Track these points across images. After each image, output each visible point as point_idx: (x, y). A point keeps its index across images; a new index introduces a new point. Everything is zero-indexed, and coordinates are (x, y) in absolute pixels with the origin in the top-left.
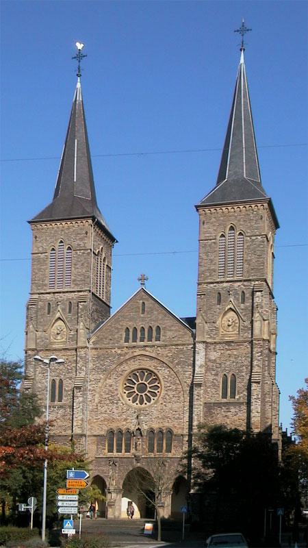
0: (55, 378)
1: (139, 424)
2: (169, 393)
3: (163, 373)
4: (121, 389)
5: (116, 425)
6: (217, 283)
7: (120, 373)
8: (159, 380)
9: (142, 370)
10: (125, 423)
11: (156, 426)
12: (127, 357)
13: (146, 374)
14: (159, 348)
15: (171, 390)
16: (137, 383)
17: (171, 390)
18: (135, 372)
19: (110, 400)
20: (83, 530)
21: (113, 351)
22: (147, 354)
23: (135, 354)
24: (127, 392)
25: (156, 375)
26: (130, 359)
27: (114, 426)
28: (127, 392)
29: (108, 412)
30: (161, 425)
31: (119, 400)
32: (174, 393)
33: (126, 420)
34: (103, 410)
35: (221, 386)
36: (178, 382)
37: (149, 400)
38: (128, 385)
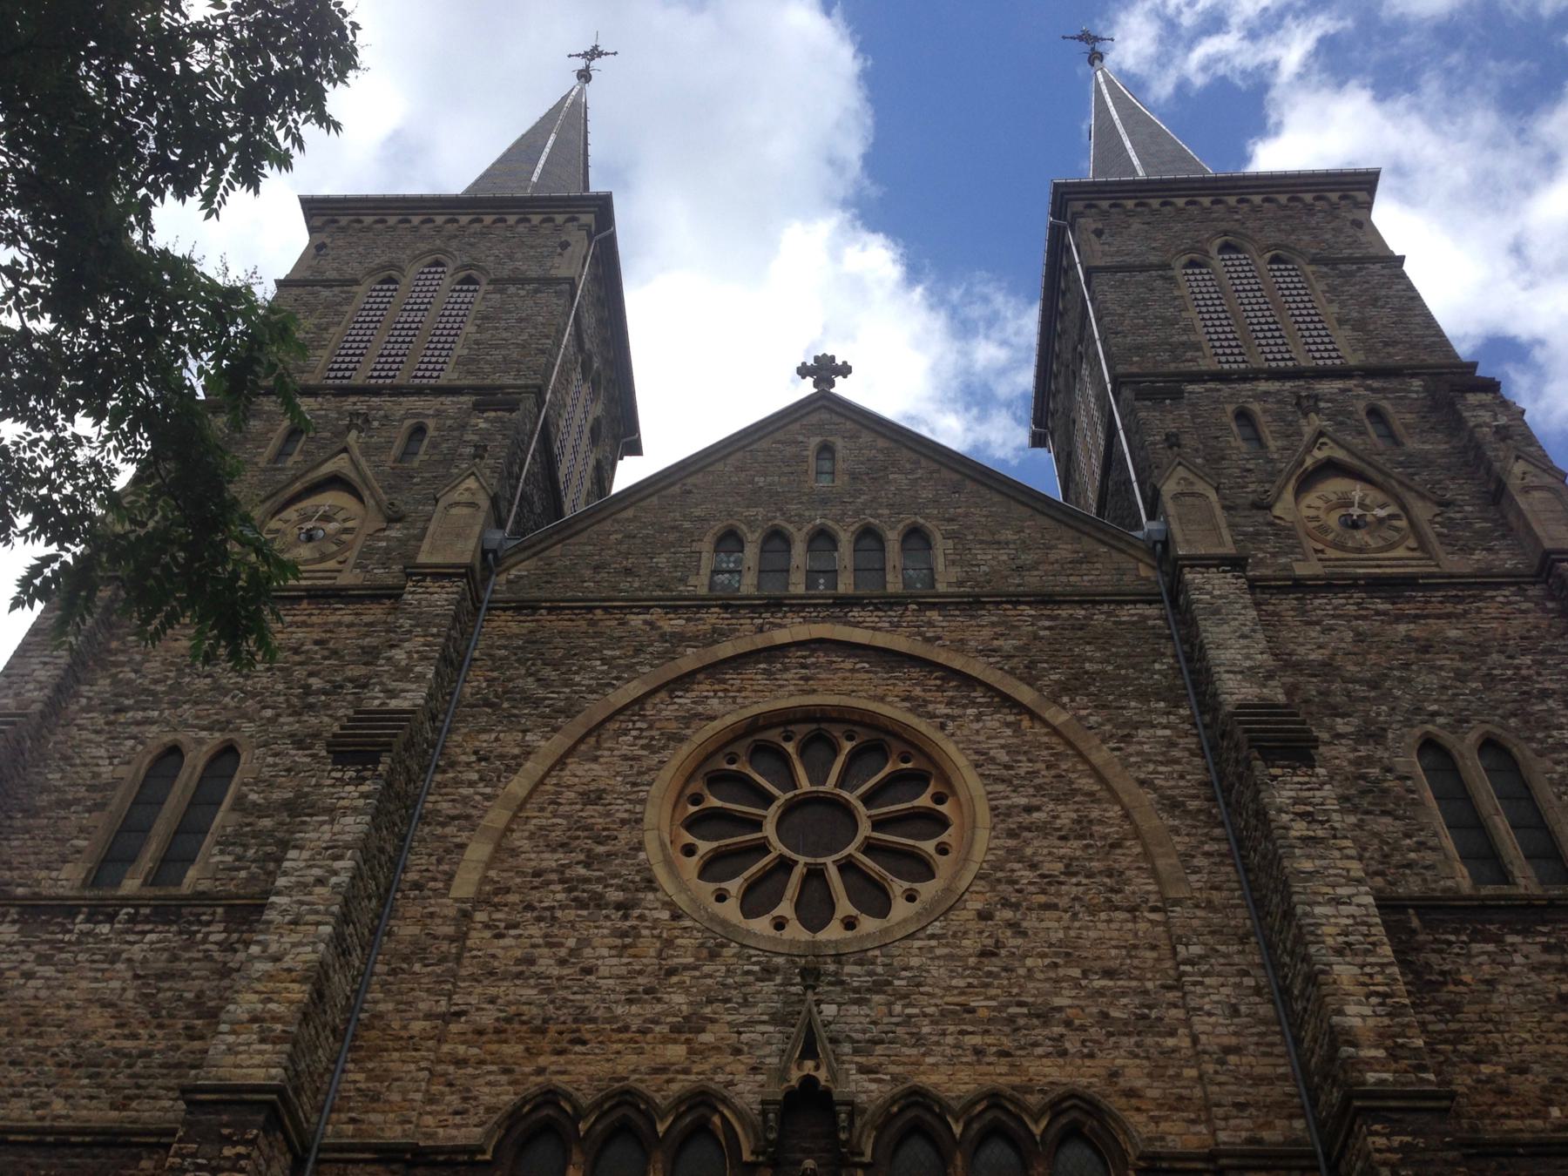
0: (184, 737)
1: (809, 1051)
2: (1036, 846)
3: (962, 742)
4: (659, 819)
5: (601, 1068)
6: (1089, 599)
7: (672, 727)
8: (946, 780)
9: (819, 730)
10: (676, 1052)
11: (953, 1080)
12: (726, 650)
13: (847, 746)
14: (934, 615)
15: (1043, 829)
16: (783, 797)
17: (1043, 829)
18: (774, 735)
19: (570, 885)
20: (1120, 369)
21: (636, 621)
22: (860, 636)
23: (781, 636)
24: (704, 847)
25: (913, 745)
26: (739, 661)
27: (583, 1074)
28: (704, 847)
29: (545, 963)
30: (999, 1075)
31: (650, 884)
32: (1073, 848)
33: (689, 1026)
34: (507, 950)
35: (1428, 794)
36: (1087, 783)
37: (875, 899)
38: (714, 802)
